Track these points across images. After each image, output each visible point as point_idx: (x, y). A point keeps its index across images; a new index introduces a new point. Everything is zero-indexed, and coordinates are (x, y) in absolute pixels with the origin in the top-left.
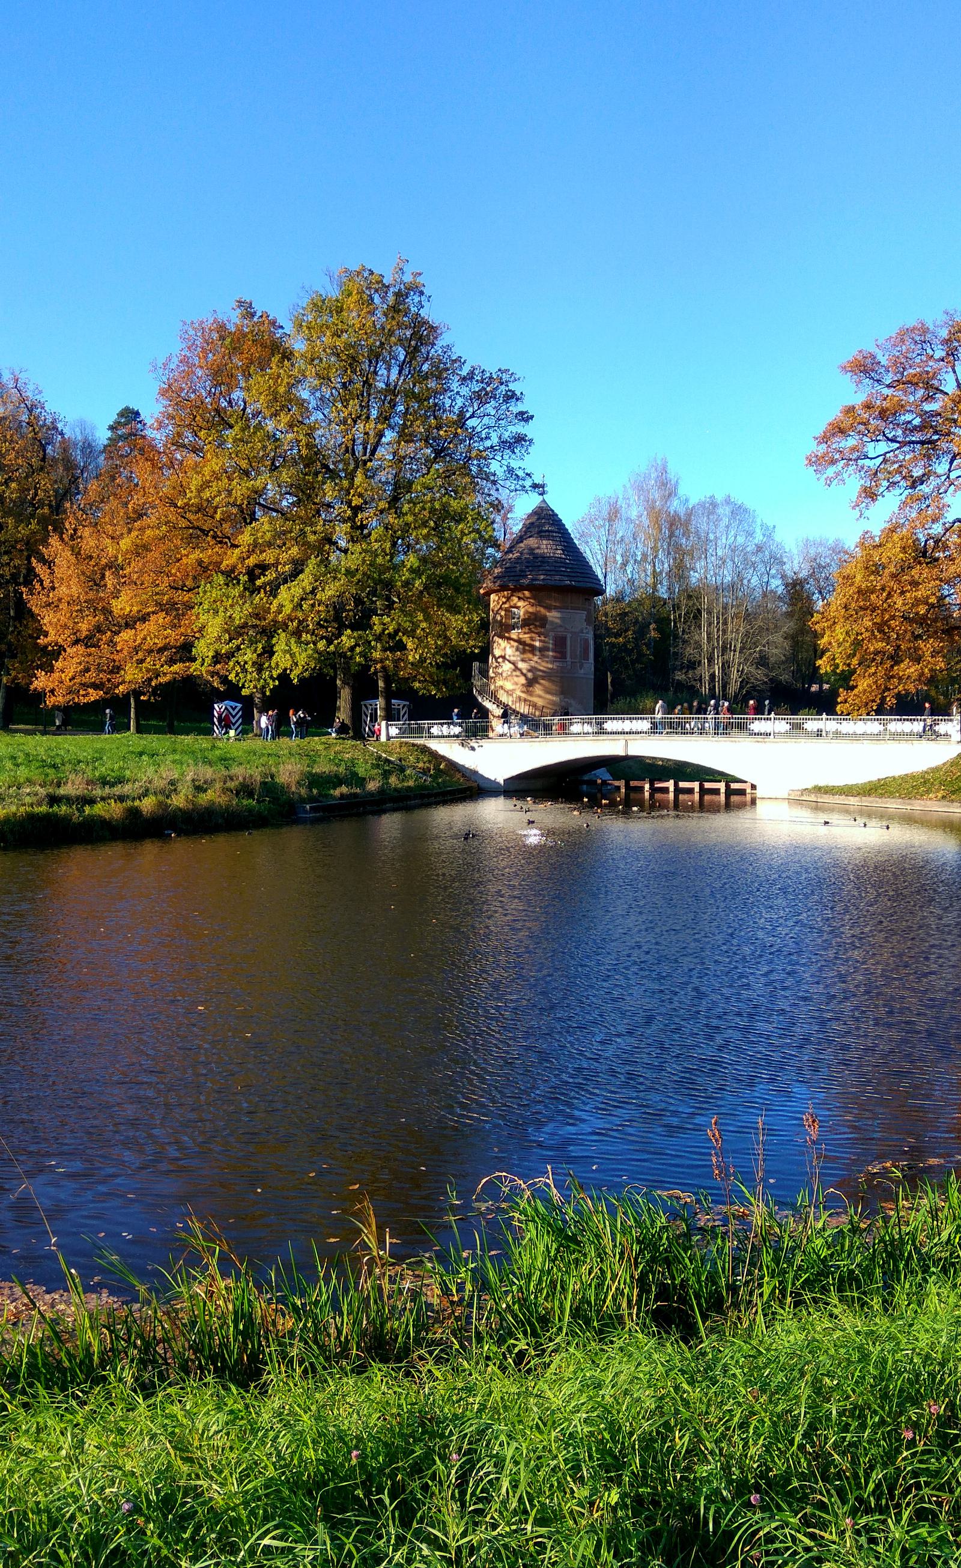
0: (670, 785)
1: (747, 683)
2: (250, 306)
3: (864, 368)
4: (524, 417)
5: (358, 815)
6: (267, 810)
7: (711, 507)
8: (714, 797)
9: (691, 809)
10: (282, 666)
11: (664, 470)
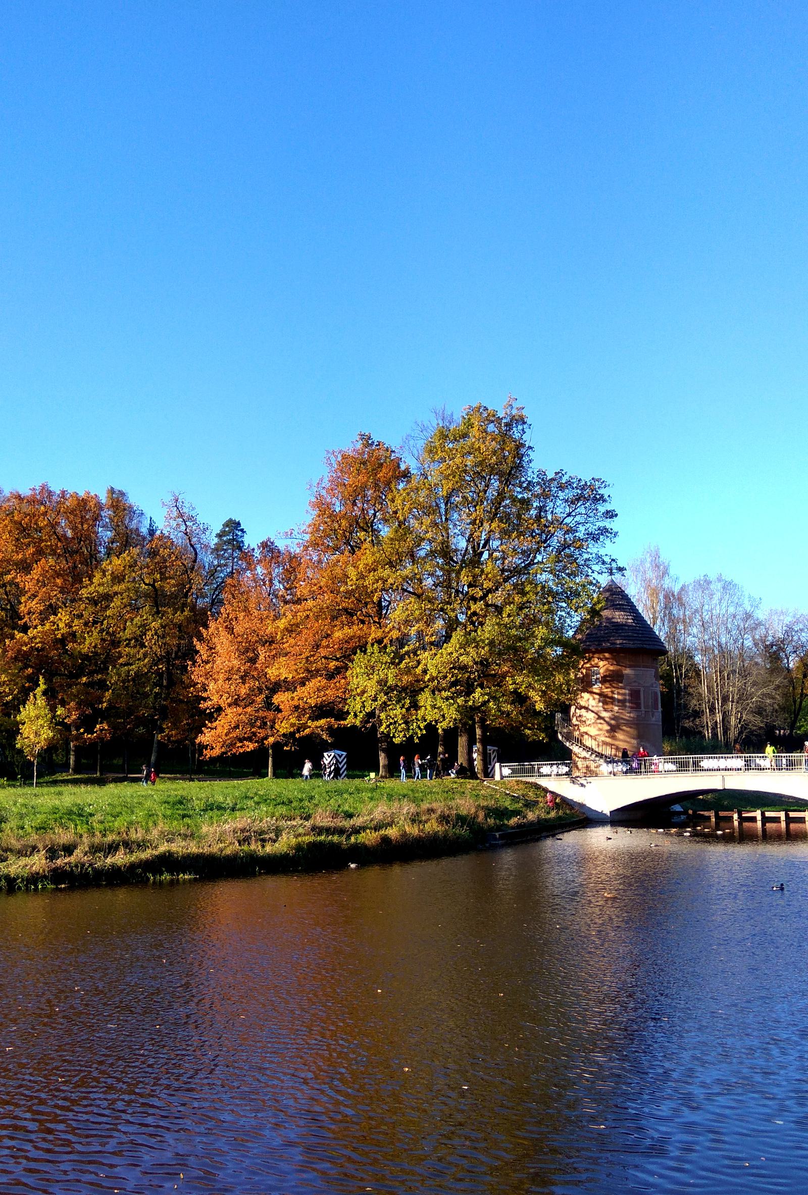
0: (758, 814)
1: (746, 728)
2: (369, 438)
4: (611, 515)
5: (527, 842)
6: (321, 858)
7: (704, 584)
8: (800, 825)
10: (429, 718)
11: (657, 556)
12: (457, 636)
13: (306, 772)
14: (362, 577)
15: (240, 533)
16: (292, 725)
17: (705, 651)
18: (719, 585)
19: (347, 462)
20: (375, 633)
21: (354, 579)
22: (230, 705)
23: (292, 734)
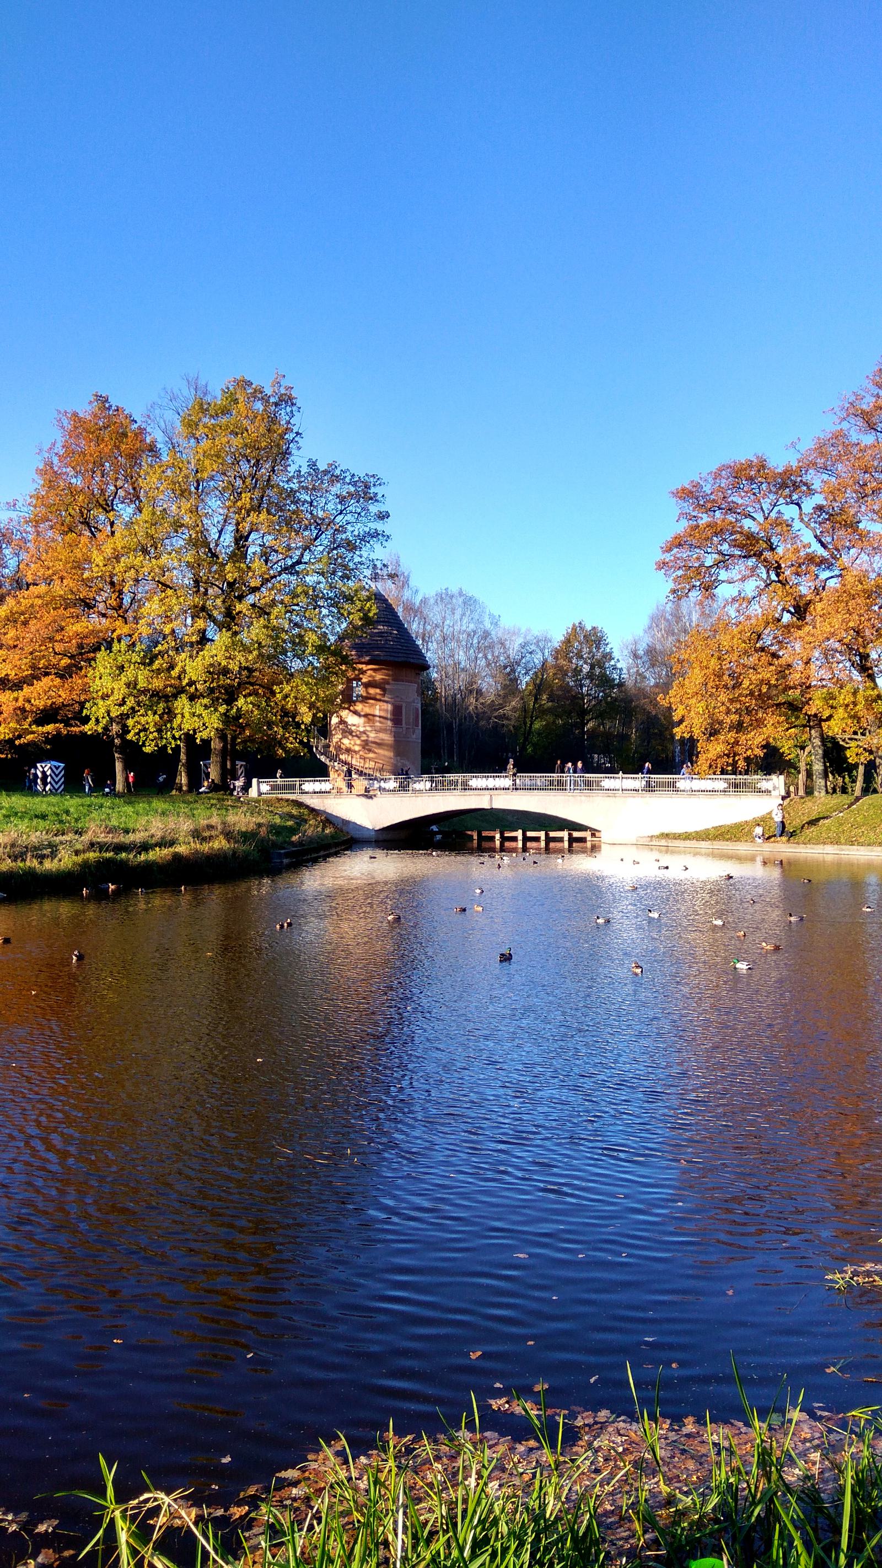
0: (519, 834)
2: (107, 401)
3: (686, 494)
4: (383, 516)
7: (445, 598)
9: (560, 851)
13: (278, 775)
17: (441, 669)
18: (461, 600)
19: (78, 426)
21: (101, 564)
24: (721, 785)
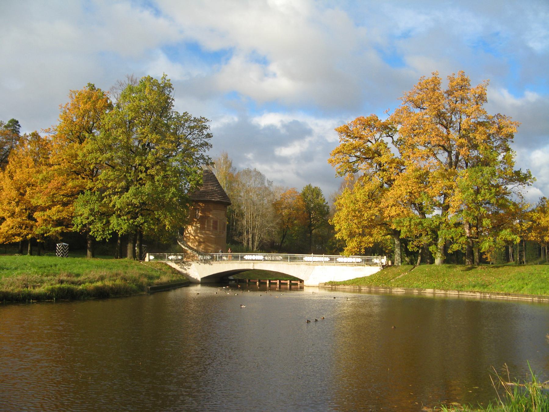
2: (94, 86)
6: (66, 296)
12: (132, 189)
14: (84, 156)
15: (17, 127)
16: (42, 230)
19: (79, 97)
20: (90, 184)
22: (9, 217)
23: (43, 234)
24: (359, 260)
